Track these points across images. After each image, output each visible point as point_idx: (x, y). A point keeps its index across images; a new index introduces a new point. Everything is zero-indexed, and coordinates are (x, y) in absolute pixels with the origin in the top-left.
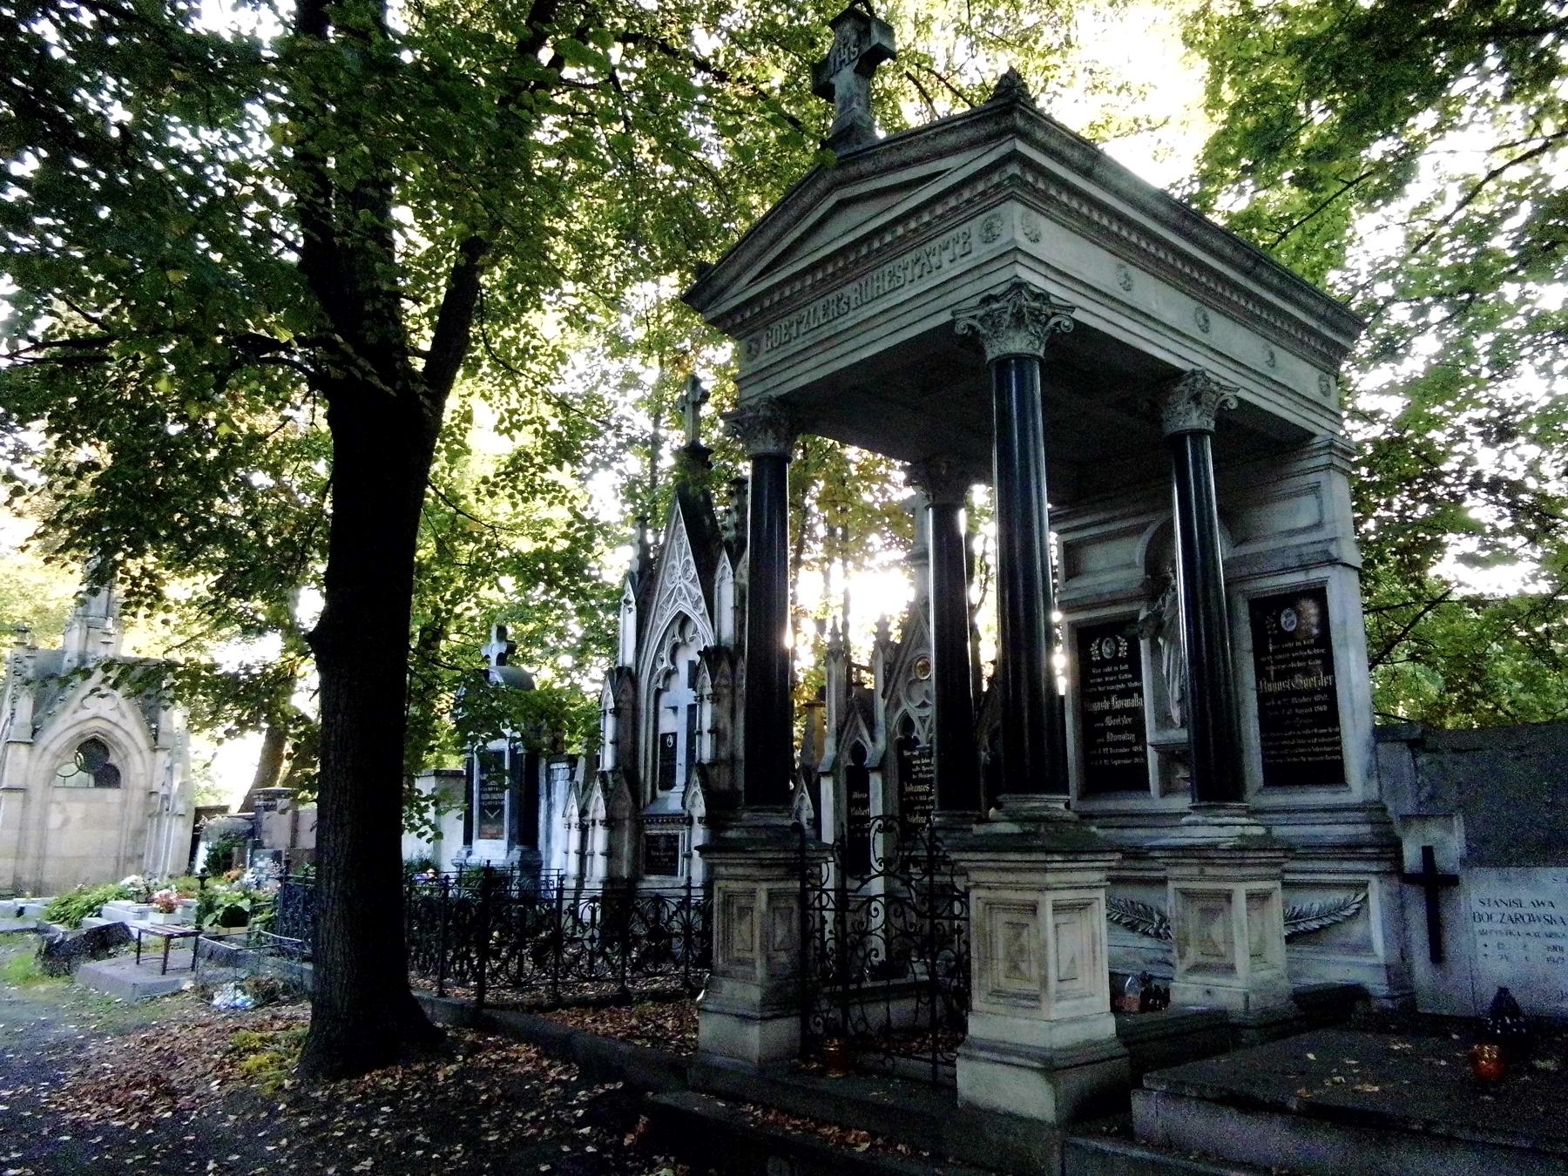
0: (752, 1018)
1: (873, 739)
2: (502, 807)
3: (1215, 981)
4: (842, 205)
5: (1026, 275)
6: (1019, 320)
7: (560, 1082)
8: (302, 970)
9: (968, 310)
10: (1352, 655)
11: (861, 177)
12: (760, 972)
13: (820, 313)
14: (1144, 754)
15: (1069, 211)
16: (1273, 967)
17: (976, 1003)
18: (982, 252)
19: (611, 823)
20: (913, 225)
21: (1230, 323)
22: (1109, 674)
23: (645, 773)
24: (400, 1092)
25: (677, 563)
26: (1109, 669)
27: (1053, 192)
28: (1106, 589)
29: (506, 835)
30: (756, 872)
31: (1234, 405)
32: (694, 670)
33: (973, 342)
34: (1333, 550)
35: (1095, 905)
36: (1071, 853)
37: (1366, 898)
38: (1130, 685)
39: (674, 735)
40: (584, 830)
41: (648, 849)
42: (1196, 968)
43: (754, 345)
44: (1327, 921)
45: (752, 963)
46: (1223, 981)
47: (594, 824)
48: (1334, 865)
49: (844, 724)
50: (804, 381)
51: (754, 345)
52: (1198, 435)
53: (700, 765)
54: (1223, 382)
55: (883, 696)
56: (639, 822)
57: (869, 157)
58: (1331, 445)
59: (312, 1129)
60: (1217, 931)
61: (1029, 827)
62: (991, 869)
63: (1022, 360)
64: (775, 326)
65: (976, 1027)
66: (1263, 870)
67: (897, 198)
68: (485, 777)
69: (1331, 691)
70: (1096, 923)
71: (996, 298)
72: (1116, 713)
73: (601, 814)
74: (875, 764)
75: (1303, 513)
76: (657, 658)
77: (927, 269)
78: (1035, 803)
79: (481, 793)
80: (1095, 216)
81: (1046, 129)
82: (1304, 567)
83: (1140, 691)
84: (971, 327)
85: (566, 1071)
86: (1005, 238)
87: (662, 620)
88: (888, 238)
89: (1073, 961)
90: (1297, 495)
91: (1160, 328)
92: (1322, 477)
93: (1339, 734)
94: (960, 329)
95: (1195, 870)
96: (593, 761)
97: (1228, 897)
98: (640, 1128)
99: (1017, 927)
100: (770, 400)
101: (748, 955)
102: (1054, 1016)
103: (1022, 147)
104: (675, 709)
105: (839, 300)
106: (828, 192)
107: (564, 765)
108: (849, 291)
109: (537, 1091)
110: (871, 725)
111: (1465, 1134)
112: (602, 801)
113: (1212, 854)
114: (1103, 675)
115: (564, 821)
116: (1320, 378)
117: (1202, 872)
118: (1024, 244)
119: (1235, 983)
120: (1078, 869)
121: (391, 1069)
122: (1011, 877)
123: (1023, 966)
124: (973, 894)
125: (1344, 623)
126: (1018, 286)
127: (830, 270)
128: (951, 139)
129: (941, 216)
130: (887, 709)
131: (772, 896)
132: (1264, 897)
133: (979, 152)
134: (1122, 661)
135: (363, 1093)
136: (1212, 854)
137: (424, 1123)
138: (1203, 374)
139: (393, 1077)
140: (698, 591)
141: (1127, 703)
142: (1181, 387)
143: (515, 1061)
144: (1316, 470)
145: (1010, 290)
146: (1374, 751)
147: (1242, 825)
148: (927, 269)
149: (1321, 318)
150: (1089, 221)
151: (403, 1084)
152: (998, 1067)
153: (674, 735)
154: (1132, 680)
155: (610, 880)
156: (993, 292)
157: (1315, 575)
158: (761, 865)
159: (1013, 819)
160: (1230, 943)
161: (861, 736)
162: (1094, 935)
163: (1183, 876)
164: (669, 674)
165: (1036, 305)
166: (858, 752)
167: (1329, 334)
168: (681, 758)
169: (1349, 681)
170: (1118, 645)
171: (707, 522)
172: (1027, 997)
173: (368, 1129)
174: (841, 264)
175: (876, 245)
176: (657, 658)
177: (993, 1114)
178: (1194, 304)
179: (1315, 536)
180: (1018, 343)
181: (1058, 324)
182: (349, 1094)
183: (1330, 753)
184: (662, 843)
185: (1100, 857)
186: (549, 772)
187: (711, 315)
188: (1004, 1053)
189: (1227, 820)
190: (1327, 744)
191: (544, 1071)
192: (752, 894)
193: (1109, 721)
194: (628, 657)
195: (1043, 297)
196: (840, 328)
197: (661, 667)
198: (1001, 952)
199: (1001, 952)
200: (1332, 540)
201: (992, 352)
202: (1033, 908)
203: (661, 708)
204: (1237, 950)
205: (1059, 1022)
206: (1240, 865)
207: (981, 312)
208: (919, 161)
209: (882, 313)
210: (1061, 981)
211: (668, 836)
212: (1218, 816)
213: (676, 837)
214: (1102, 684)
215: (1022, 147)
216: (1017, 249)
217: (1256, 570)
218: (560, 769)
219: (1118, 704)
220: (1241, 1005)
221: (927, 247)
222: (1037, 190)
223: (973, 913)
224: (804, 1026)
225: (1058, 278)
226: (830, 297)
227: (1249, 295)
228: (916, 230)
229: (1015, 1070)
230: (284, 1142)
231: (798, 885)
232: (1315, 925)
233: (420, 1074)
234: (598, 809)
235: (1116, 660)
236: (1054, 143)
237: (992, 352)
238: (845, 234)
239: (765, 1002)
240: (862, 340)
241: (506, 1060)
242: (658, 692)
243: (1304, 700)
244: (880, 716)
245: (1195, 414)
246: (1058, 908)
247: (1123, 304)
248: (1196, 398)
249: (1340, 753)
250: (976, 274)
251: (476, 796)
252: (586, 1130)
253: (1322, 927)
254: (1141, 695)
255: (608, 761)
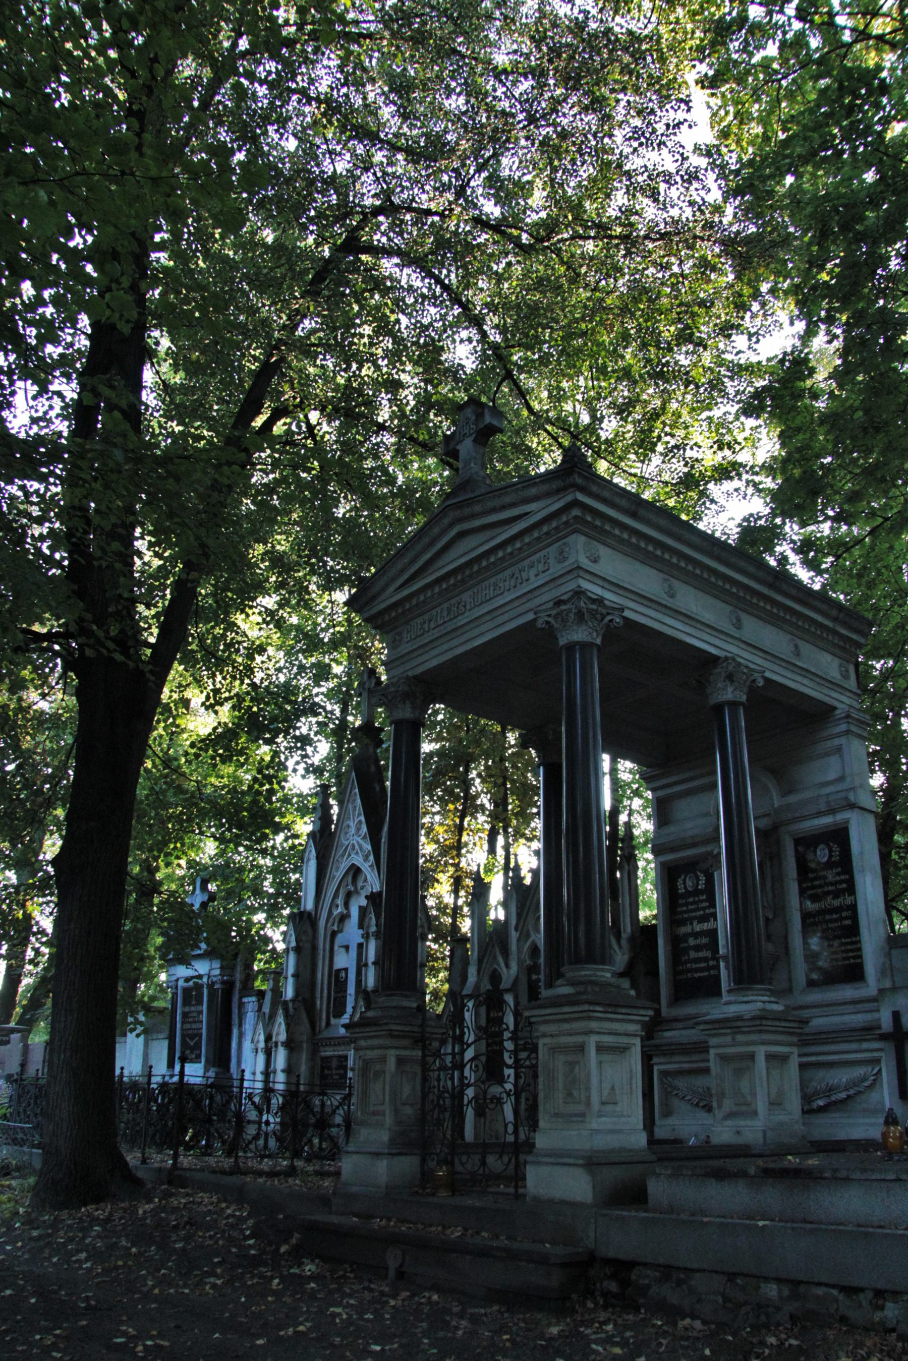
0: (383, 1154)
1: (507, 966)
2: (201, 1035)
3: (742, 1123)
4: (462, 535)
5: (585, 585)
6: (580, 617)
7: (233, 1216)
8: (31, 1154)
9: (545, 611)
10: (868, 879)
11: (473, 516)
12: (389, 1120)
13: (445, 614)
14: (717, 967)
15: (621, 541)
16: (790, 1114)
17: (541, 1124)
18: (556, 569)
19: (289, 1045)
20: (509, 550)
21: (760, 623)
22: (692, 903)
23: (321, 1003)
24: (108, 1220)
25: (351, 824)
26: (691, 900)
27: (607, 527)
28: (690, 833)
29: (203, 1060)
30: (388, 1042)
31: (761, 683)
32: (363, 911)
33: (550, 633)
34: (852, 797)
35: (633, 1049)
36: (610, 1005)
37: (880, 1070)
38: (707, 911)
39: (346, 970)
40: (268, 1053)
41: (323, 1068)
42: (730, 1115)
43: (397, 638)
44: (852, 1092)
45: (384, 1114)
46: (749, 1123)
47: (276, 1046)
48: (854, 1046)
49: (483, 957)
50: (435, 663)
51: (397, 638)
52: (734, 705)
53: (365, 992)
54: (752, 666)
55: (516, 929)
56: (316, 1045)
57: (479, 501)
58: (848, 716)
59: (40, 1237)
60: (745, 1084)
61: (580, 988)
62: (553, 1021)
63: (584, 646)
64: (413, 623)
65: (541, 1141)
66: (781, 1038)
67: (499, 530)
68: (187, 1009)
69: (853, 908)
70: (633, 1062)
71: (564, 602)
72: (696, 935)
73: (283, 1037)
74: (508, 986)
75: (831, 769)
76: (333, 905)
77: (519, 581)
78: (587, 972)
79: (183, 1023)
80: (643, 545)
81: (599, 485)
82: (832, 811)
83: (714, 916)
84: (547, 623)
85: (240, 1210)
86: (572, 560)
87: (338, 872)
88: (492, 559)
89: (613, 1088)
90: (827, 754)
91: (698, 626)
92: (843, 740)
93: (859, 942)
94: (540, 624)
95: (728, 1039)
96: (277, 992)
97: (752, 1057)
98: (294, 1241)
99: (572, 1064)
100: (407, 677)
101: (381, 1108)
102: (594, 1126)
103: (581, 497)
104: (347, 948)
105: (459, 603)
106: (451, 525)
107: (254, 999)
108: (466, 597)
109: (216, 1221)
110: (506, 953)
111: (857, 1175)
112: (283, 1026)
113: (739, 1024)
114: (687, 904)
115: (253, 1046)
116: (841, 666)
117: (733, 1039)
118: (584, 562)
119: (758, 1123)
120: (618, 1020)
121: (102, 1205)
122: (566, 1026)
123: (575, 1093)
124: (541, 1042)
125: (862, 853)
126: (579, 593)
127: (452, 581)
128: (533, 491)
129: (529, 544)
130: (518, 940)
131: (400, 1061)
132: (783, 1059)
133: (549, 501)
134: (701, 892)
135: (80, 1219)
136: (739, 1024)
137: (127, 1236)
138: (733, 659)
139: (104, 1211)
140: (368, 847)
141: (705, 926)
142: (719, 670)
143: (200, 1203)
144: (839, 735)
145: (572, 597)
146: (889, 955)
147: (764, 1002)
148: (519, 581)
149: (835, 619)
150: (637, 548)
151: (111, 1214)
152: (557, 1168)
153: (346, 970)
154: (709, 907)
155: (291, 1094)
156: (563, 598)
157: (840, 817)
158: (391, 1035)
159: (572, 984)
160: (754, 1095)
161: (499, 965)
162: (631, 1071)
163: (719, 1045)
164: (343, 918)
165: (594, 607)
166: (495, 978)
167: (844, 632)
168: (351, 989)
169: (866, 899)
170: (698, 879)
171: (378, 788)
172: (576, 1115)
173: (84, 1238)
174: (459, 578)
175: (484, 563)
176: (333, 905)
177: (551, 1202)
178: (728, 608)
179: (840, 787)
180: (579, 634)
181: (611, 621)
182: (69, 1219)
183: (854, 957)
184: (334, 1064)
185: (635, 1011)
186: (241, 1005)
187: (366, 615)
188: (559, 1157)
189: (752, 998)
190: (852, 951)
191: (223, 1210)
192: (383, 1060)
193: (692, 942)
194: (309, 904)
195: (600, 601)
196: (459, 624)
197: (336, 912)
198: (560, 1085)
199: (560, 1085)
200: (851, 789)
201: (562, 642)
202: (581, 1048)
203: (336, 948)
204: (759, 1097)
205: (598, 1131)
206: (760, 1031)
207: (553, 612)
208: (513, 505)
209: (487, 613)
210: (603, 1103)
211: (340, 1057)
212: (745, 996)
213: (346, 1058)
214: (686, 912)
215: (581, 497)
216: (579, 568)
217: (797, 815)
218: (251, 1002)
219: (698, 927)
220: (761, 1141)
221: (520, 566)
222: (596, 527)
223: (540, 1056)
224: (423, 1161)
225: (613, 588)
226: (453, 601)
227: (774, 602)
228: (511, 554)
229: (565, 1168)
230: (20, 1244)
231: (420, 1053)
232: (843, 1095)
233: (125, 1210)
234: (281, 1033)
235: (696, 892)
236: (606, 494)
237: (562, 642)
238: (461, 556)
239: (392, 1141)
240: (476, 632)
241: (190, 1202)
242: (334, 934)
243: (835, 916)
244: (514, 947)
245: (730, 689)
246: (600, 1049)
247: (670, 608)
248: (730, 677)
249: (860, 957)
250: (552, 585)
251: (179, 1025)
252: (251, 1242)
253: (849, 1097)
254: (715, 919)
255: (289, 992)
